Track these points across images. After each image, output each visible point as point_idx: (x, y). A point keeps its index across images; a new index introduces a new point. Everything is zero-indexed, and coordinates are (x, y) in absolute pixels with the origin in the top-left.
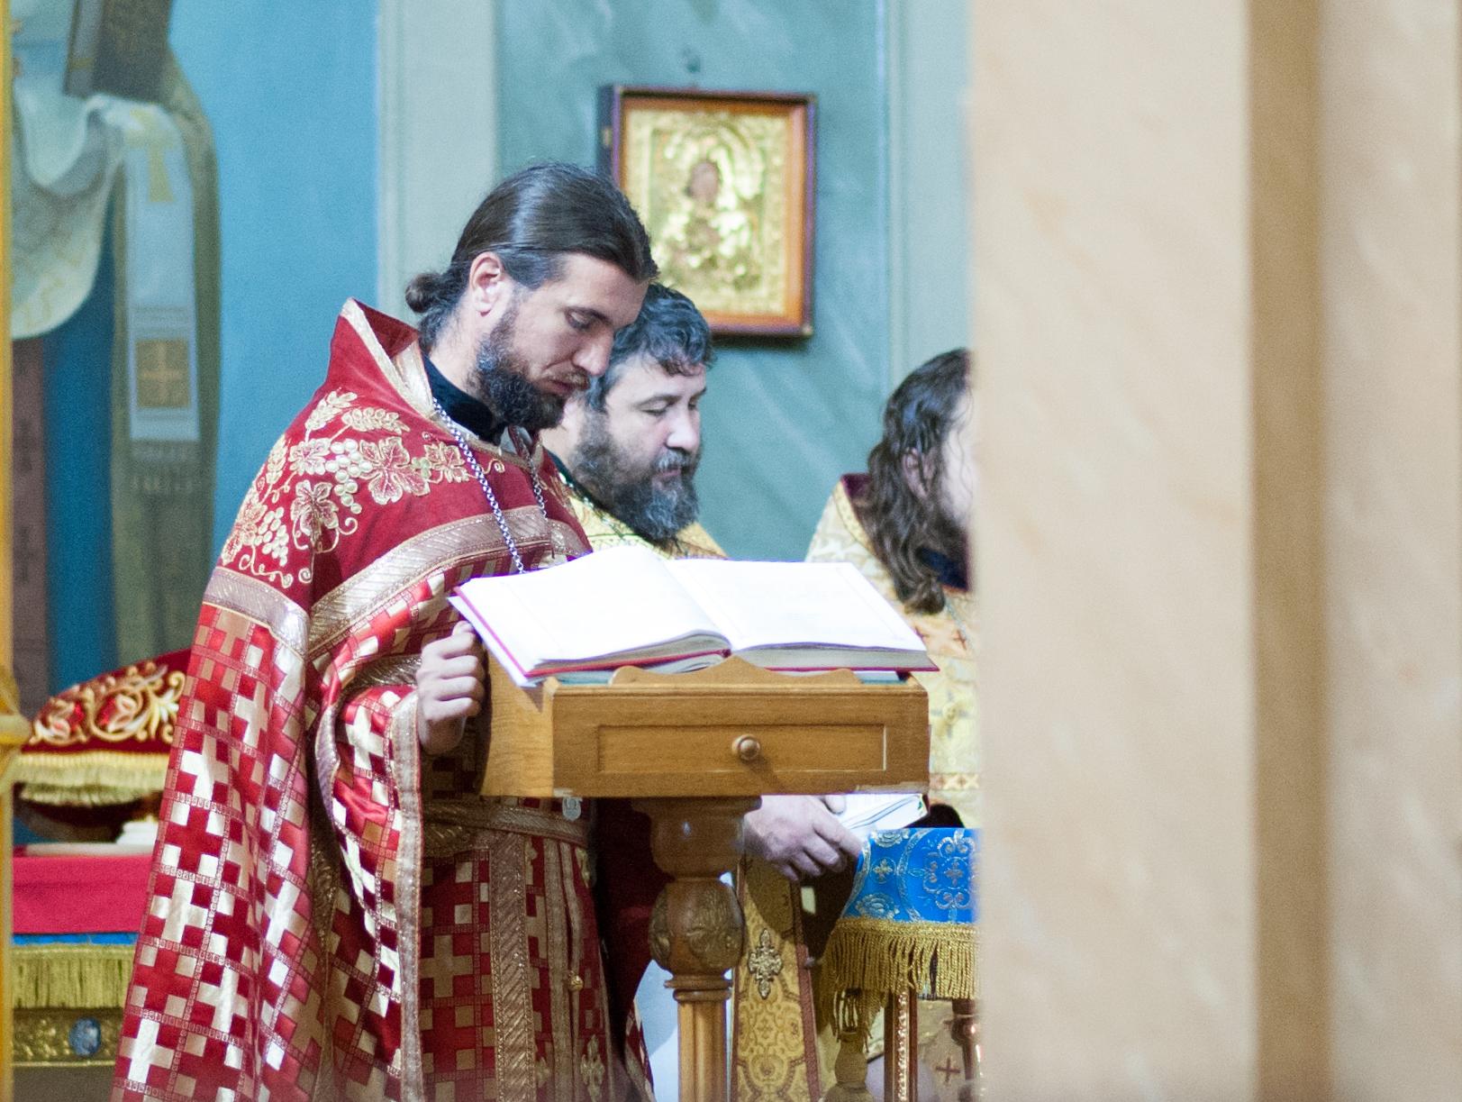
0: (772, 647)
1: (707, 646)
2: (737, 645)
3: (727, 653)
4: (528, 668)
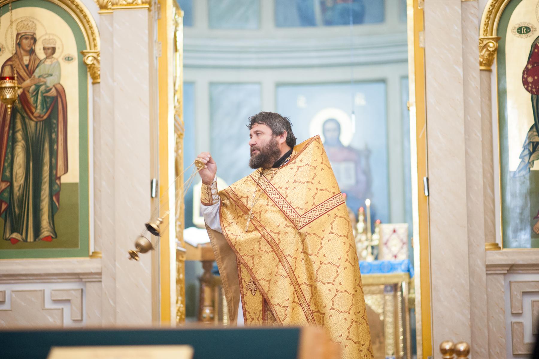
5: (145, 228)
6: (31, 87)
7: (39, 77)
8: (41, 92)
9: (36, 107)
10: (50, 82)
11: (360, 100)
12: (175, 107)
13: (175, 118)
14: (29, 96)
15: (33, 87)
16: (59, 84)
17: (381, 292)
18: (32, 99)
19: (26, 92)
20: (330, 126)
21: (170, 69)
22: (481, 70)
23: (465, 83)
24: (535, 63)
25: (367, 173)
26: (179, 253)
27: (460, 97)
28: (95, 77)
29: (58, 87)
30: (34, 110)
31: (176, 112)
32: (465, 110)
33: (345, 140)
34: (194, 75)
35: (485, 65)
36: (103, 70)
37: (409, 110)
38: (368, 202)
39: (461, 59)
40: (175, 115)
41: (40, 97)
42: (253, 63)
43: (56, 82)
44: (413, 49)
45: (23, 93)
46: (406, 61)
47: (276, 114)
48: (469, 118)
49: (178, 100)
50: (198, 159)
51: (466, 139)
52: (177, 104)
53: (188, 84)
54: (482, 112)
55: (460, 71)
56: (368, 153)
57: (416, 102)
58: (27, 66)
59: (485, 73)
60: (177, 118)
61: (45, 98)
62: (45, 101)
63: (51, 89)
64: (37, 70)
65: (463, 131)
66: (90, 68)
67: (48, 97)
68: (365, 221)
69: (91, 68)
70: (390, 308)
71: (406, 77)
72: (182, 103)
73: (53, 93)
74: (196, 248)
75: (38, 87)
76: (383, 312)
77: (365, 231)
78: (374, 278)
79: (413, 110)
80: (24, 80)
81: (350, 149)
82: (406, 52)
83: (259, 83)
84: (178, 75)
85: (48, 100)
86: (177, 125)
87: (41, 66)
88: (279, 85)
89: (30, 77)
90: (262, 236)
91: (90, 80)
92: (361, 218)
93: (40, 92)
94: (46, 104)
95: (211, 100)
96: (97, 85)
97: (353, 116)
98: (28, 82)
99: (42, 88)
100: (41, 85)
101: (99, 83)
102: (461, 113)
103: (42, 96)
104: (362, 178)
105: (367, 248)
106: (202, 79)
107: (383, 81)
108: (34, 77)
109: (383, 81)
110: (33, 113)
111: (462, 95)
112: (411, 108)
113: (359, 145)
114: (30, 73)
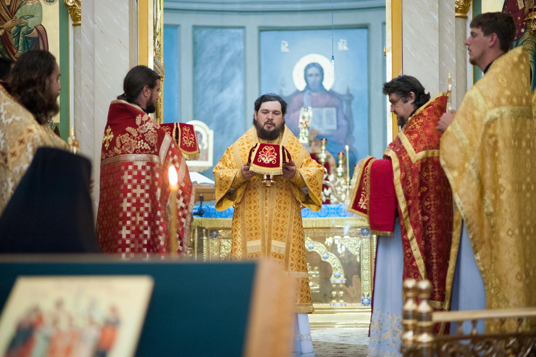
6: (13, 27)
7: (21, 18)
8: (23, 33)
9: (18, 48)
10: (31, 23)
11: (342, 46)
12: (155, 50)
13: (154, 60)
14: (11, 37)
15: (15, 28)
16: (41, 25)
18: (14, 40)
19: (8, 33)
20: (312, 70)
21: (151, 11)
22: (456, 17)
23: (441, 30)
24: (511, 10)
25: (349, 118)
27: (435, 43)
28: (76, 19)
29: (39, 28)
30: (15, 51)
31: (156, 54)
32: (439, 56)
33: (328, 84)
34: (175, 19)
35: (461, 11)
36: (84, 11)
37: (385, 55)
38: (347, 147)
39: (437, 6)
40: (154, 58)
41: (21, 38)
43: (37, 24)
45: (5, 34)
46: (384, 7)
47: (415, 79)
48: (444, 64)
49: (158, 42)
51: (440, 85)
52: (157, 47)
53: (170, 28)
54: (457, 59)
55: (436, 17)
56: (349, 98)
58: (9, 7)
59: (460, 19)
60: (156, 59)
61: (26, 39)
62: (27, 42)
63: (33, 30)
64: (19, 11)
65: (437, 77)
66: (70, 9)
67: (29, 38)
68: (344, 164)
69: (72, 9)
70: (366, 251)
71: (384, 23)
72: (162, 46)
73: (35, 34)
75: (19, 28)
77: (344, 175)
79: (389, 55)
80: (6, 21)
81: (331, 93)
84: (159, 17)
85: (29, 41)
86: (157, 67)
87: (23, 7)
88: (262, 30)
89: (12, 19)
90: (497, 302)
91: (71, 22)
92: (341, 162)
93: (21, 32)
94: (27, 46)
95: (195, 43)
96: (78, 27)
97: (333, 61)
98: (9, 23)
99: (24, 29)
100: (23, 26)
101: (80, 24)
102: (436, 60)
103: (23, 37)
104: (344, 123)
105: (345, 192)
106: (186, 23)
107: (366, 27)
108: (16, 17)
109: (366, 27)
110: (14, 54)
111: (437, 42)
112: (387, 54)
113: (340, 90)
114: (11, 14)
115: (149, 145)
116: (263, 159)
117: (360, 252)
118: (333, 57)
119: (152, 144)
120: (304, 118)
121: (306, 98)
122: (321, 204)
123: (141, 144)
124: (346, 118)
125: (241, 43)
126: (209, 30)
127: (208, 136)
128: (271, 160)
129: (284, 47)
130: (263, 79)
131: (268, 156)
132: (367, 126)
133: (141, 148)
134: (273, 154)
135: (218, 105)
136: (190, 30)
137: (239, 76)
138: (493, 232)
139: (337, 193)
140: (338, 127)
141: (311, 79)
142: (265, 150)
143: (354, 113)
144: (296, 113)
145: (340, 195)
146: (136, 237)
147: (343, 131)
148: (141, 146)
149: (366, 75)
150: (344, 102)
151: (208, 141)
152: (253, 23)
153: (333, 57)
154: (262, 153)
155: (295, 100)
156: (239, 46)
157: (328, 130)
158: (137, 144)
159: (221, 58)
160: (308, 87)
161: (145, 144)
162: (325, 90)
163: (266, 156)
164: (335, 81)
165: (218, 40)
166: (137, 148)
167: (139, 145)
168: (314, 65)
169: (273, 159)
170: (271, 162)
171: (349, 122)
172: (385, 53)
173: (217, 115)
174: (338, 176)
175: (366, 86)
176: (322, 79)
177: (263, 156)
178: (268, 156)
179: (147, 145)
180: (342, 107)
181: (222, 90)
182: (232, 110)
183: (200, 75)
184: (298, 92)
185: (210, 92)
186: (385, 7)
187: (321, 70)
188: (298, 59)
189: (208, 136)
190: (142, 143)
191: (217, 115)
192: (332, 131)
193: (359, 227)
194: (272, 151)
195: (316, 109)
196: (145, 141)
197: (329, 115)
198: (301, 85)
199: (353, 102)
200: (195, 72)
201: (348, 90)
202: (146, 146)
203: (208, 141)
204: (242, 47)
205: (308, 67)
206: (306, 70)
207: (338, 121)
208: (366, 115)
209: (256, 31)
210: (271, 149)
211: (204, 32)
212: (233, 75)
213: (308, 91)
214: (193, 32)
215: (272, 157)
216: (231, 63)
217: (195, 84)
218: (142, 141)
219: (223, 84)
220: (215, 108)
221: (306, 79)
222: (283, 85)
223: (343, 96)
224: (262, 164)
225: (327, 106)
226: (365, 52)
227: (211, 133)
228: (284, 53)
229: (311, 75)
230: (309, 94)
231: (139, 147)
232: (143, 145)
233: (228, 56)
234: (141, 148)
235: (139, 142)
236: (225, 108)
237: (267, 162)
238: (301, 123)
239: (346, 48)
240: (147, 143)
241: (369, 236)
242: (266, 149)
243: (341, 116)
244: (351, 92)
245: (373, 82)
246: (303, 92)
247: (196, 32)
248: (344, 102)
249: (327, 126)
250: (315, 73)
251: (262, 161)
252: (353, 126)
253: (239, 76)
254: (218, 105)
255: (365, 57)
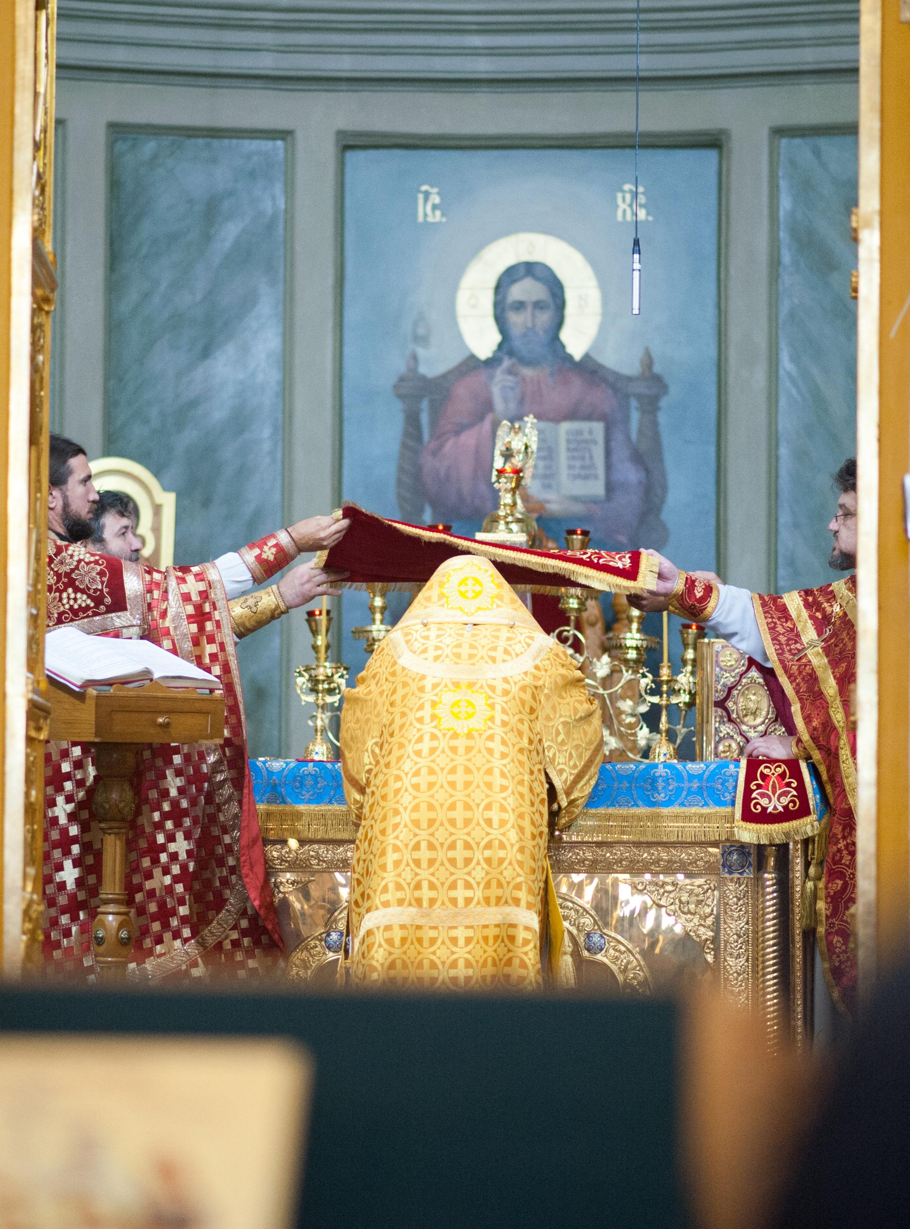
0: (167, 677)
1: (146, 674)
2: (156, 675)
3: (152, 680)
4: (79, 684)
5: (310, 647)
11: (627, 207)
17: (710, 869)
21: (24, 65)
25: (648, 458)
26: (36, 713)
37: (856, 240)
42: (266, 63)
44: (877, 97)
46: (853, 71)
50: (674, 391)
56: (652, 385)
57: (882, 213)
70: (736, 925)
74: (80, 696)
76: (715, 940)
78: (688, 818)
81: (588, 369)
82: (854, 40)
83: (284, 135)
88: (350, 143)
95: (114, 185)
97: (636, 256)
104: (630, 474)
107: (712, 141)
109: (712, 141)
113: (621, 360)
115: (89, 596)
116: (764, 802)
117: (717, 931)
118: (636, 242)
119: (96, 590)
120: (508, 455)
121: (499, 386)
122: (323, 650)
123: (69, 598)
124: (638, 458)
125: (279, 189)
126: (166, 140)
127: (157, 510)
128: (785, 800)
129: (428, 209)
130: (351, 314)
131: (774, 793)
132: (710, 489)
133: (71, 607)
134: (788, 785)
135: (194, 404)
136: (101, 136)
137: (266, 306)
138: (546, 476)
139: (620, 723)
140: (610, 487)
141: (517, 320)
142: (764, 777)
143: (667, 439)
144: (469, 438)
145: (630, 726)
146: (163, 927)
147: (628, 503)
148: (72, 602)
149: (711, 312)
150: (634, 403)
151: (156, 530)
152: (318, 120)
153: (636, 242)
154: (759, 786)
155: (462, 391)
156: (272, 200)
157: (575, 499)
158: (61, 600)
159: (207, 238)
160: (505, 347)
161: (79, 595)
162: (569, 358)
163: (770, 793)
164: (603, 329)
165: (195, 176)
166: (62, 609)
167: (65, 601)
168: (530, 269)
169: (789, 798)
170: (786, 807)
171: (647, 471)
172: (855, 230)
173: (188, 437)
174: (626, 661)
175: (712, 352)
176: (559, 322)
177: (763, 795)
178: (774, 793)
179: (85, 597)
180: (627, 419)
181: (206, 353)
182: (240, 421)
183: (132, 296)
184: (471, 364)
185: (165, 360)
186: (855, 71)
187: (556, 290)
188: (475, 251)
189: (157, 510)
190: (72, 596)
191: (188, 437)
192: (595, 501)
193: (715, 844)
194: (782, 776)
195: (543, 425)
196: (76, 590)
197: (578, 446)
198: (483, 339)
199: (664, 402)
200: (114, 286)
201: (648, 361)
202: (83, 600)
203: (156, 530)
204: (281, 204)
205: (510, 276)
206: (500, 288)
207: (608, 467)
208: (712, 449)
209: (329, 149)
210: (780, 771)
211: (149, 147)
212: (248, 302)
213: (507, 363)
214: (111, 146)
215: (785, 794)
216: (243, 256)
217: (113, 327)
218: (70, 590)
219: (211, 330)
220: (183, 414)
221: (500, 319)
222: (422, 340)
223: (629, 379)
224: (765, 817)
225: (572, 415)
226: (709, 229)
227: (168, 501)
228: (426, 223)
229: (520, 306)
230: (510, 372)
231: (67, 606)
232: (75, 599)
233: (230, 232)
234: (71, 607)
235: (65, 595)
236: (218, 412)
237: (775, 808)
238: (501, 472)
239: (642, 214)
240: (83, 592)
241: (749, 874)
242: (766, 771)
243: (621, 453)
244: (657, 369)
245: (735, 334)
246: (491, 363)
247: (120, 146)
248: (634, 403)
249: (574, 487)
250: (531, 297)
251: (764, 809)
252: (664, 488)
253: (266, 306)
254: (194, 404)
255: (710, 248)
